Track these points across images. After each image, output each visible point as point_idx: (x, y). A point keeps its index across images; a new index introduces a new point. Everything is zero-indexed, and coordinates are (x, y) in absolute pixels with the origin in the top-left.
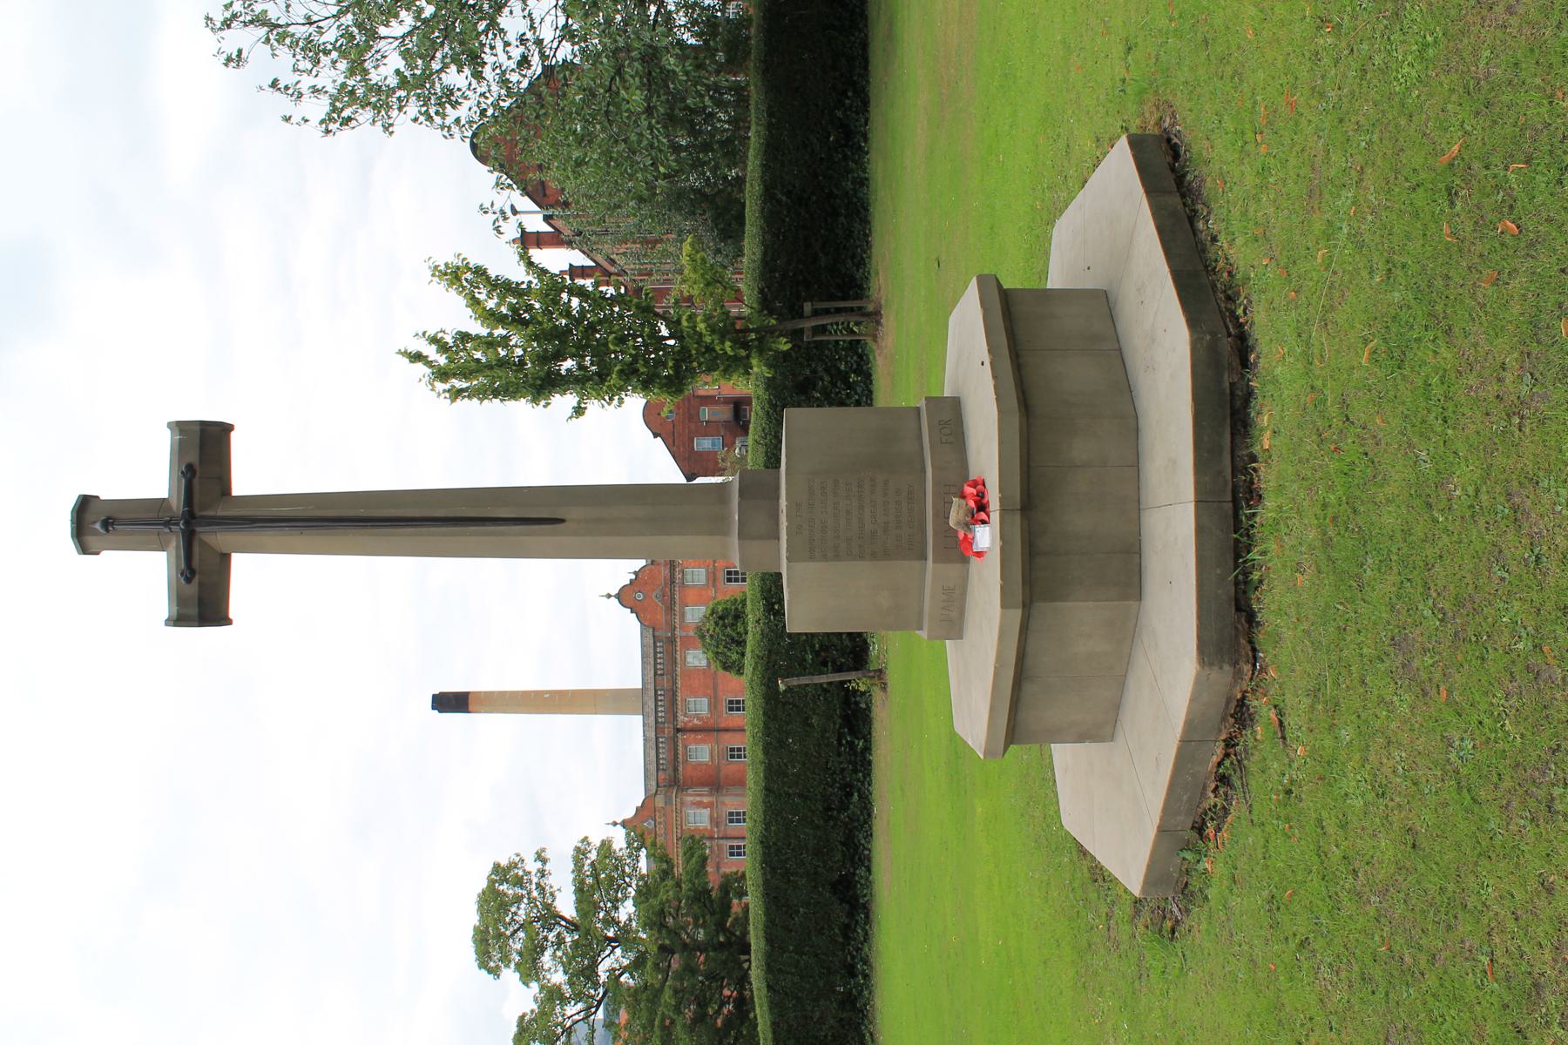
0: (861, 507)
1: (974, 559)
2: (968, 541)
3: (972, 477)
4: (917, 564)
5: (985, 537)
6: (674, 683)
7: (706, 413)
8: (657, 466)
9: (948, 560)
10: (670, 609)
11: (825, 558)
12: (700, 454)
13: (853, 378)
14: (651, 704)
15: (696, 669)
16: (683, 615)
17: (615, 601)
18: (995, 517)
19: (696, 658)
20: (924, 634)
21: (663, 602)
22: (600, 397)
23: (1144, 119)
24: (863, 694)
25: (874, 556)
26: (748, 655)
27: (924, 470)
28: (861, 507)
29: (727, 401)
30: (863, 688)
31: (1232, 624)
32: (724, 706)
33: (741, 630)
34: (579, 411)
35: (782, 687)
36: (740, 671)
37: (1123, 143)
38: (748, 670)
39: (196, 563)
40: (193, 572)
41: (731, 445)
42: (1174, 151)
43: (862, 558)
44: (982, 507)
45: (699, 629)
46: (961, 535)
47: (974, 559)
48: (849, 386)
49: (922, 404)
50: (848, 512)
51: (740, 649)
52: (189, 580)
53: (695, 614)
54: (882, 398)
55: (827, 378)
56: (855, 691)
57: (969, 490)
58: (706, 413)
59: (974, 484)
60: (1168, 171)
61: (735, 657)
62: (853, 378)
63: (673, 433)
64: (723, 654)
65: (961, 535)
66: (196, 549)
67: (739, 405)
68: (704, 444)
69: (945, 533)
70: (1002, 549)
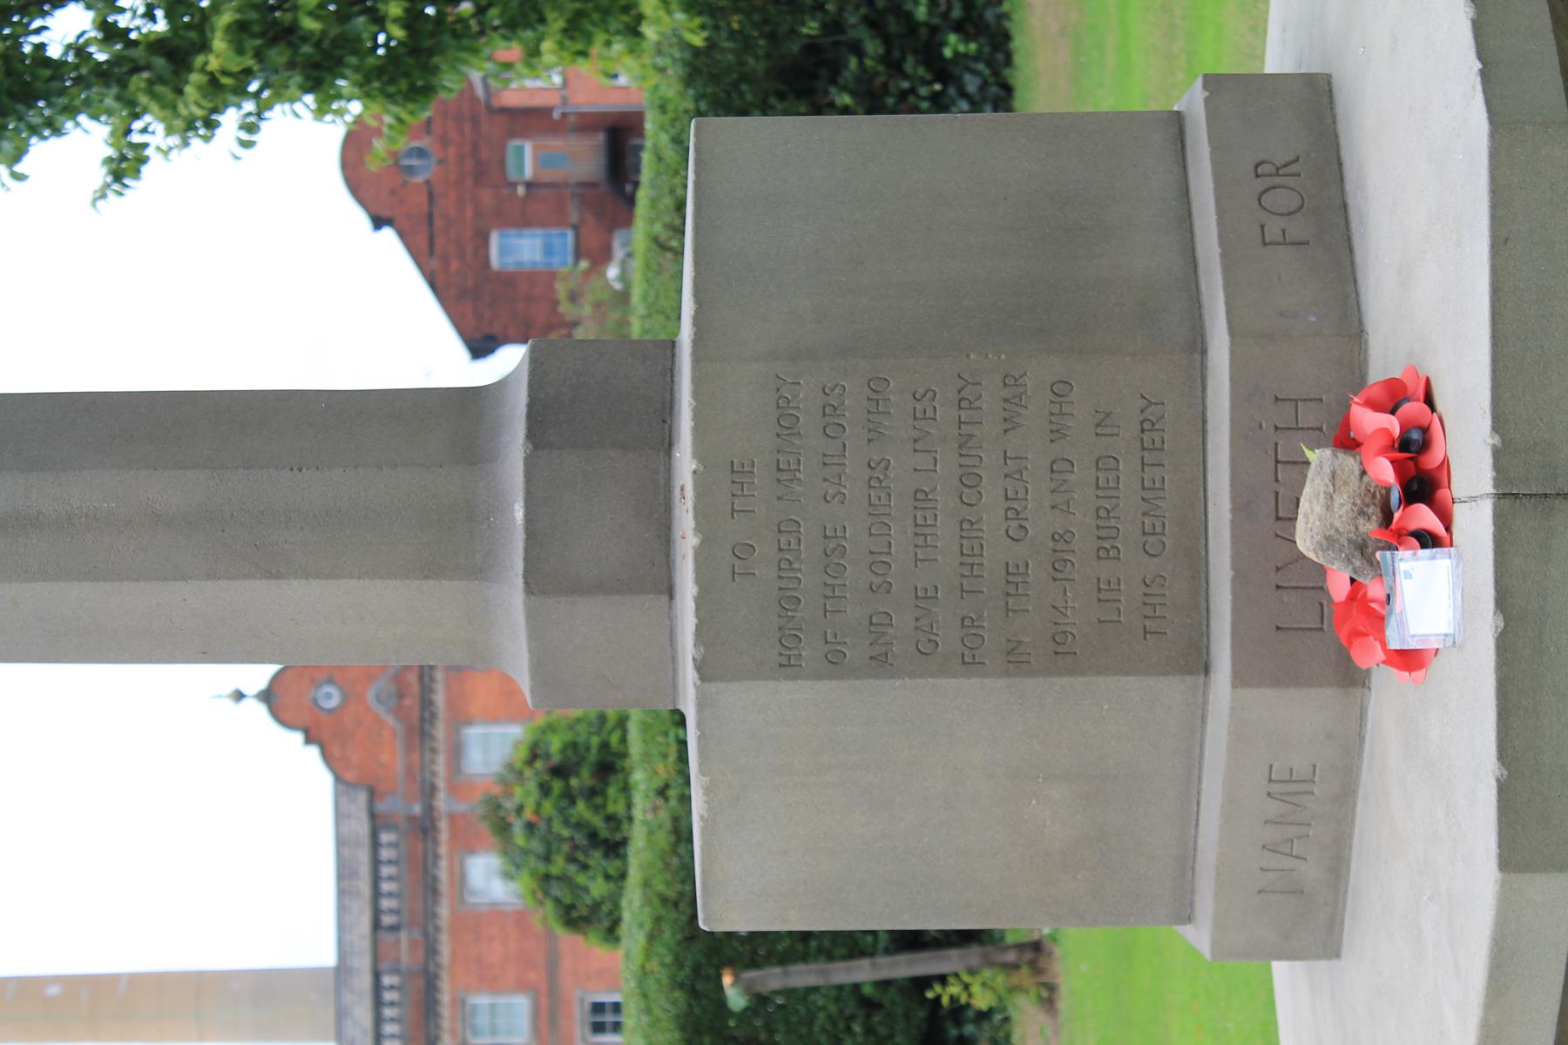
0: (969, 479)
1: (1387, 684)
2: (1367, 613)
3: (1383, 365)
4: (1172, 689)
5: (1436, 595)
6: (431, 951)
7: (527, 159)
8: (377, 325)
9: (1286, 675)
10: (420, 731)
11: (835, 665)
12: (508, 280)
13: (953, 44)
14: (362, 1013)
15: (496, 913)
16: (457, 751)
17: (261, 710)
18: (1475, 521)
19: (488, 879)
20: (1199, 936)
21: (398, 711)
22: (113, 134)
24: (984, 1016)
25: (1016, 661)
26: (634, 875)
27: (1198, 346)
28: (969, 479)
29: (587, 123)
30: (982, 1001)
32: (578, 1021)
33: (616, 807)
34: (125, 166)
35: (736, 999)
36: (612, 933)
38: (633, 935)
41: (602, 256)
43: (970, 663)
44: (1422, 483)
45: (494, 805)
46: (1339, 587)
47: (1387, 684)
48: (944, 72)
49: (1192, 101)
50: (921, 497)
51: (613, 866)
53: (491, 748)
54: (1045, 75)
55: (873, 47)
56: (958, 1011)
57: (1370, 421)
58: (527, 159)
59: (1392, 397)
61: (598, 888)
62: (953, 44)
63: (435, 214)
64: (563, 879)
65: (1339, 587)
67: (619, 137)
68: (519, 249)
69: (1278, 573)
70: (1503, 645)
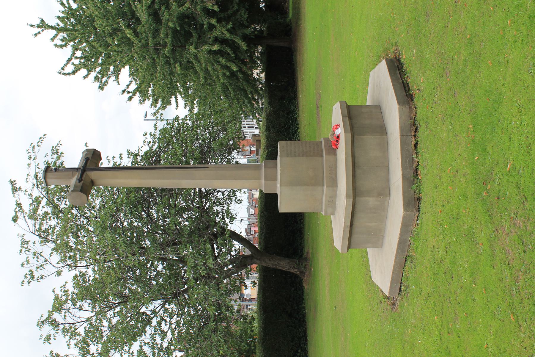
11: (292, 157)
23: (391, 56)
31: (414, 202)
34: (241, 233)
37: (384, 62)
39: (83, 178)
40: (82, 180)
42: (399, 60)
52: (80, 181)
60: (396, 67)
66: (85, 175)
